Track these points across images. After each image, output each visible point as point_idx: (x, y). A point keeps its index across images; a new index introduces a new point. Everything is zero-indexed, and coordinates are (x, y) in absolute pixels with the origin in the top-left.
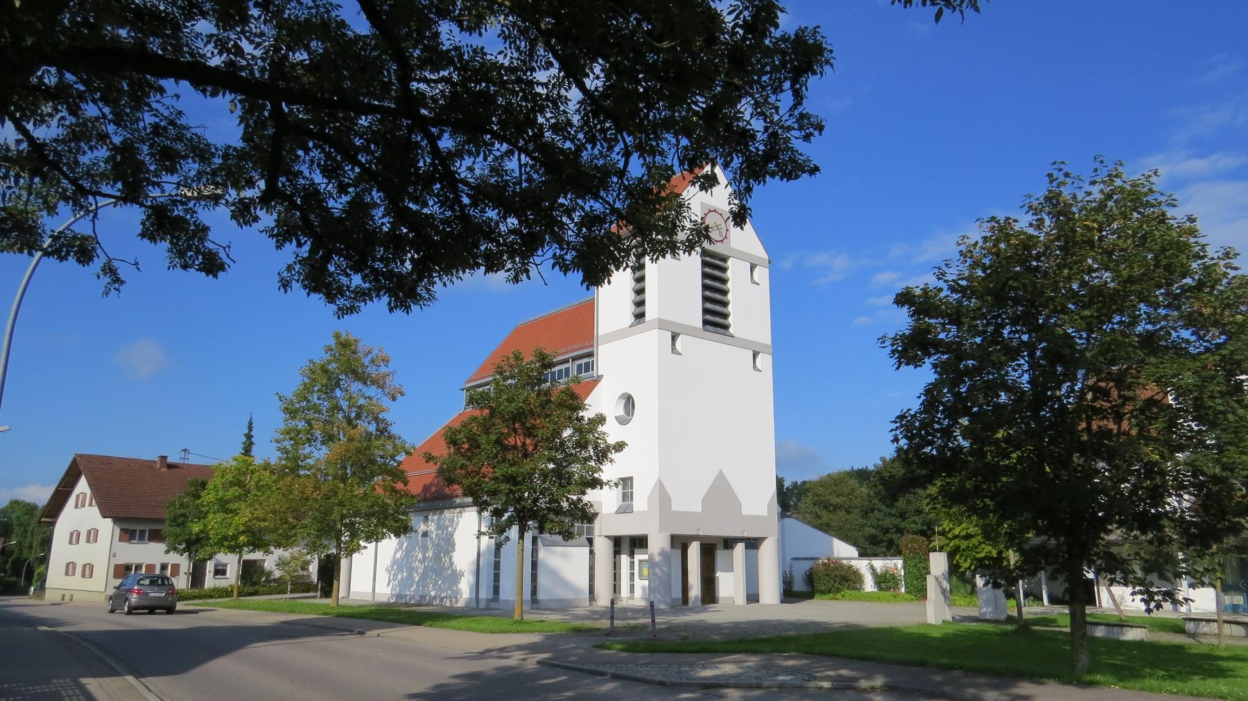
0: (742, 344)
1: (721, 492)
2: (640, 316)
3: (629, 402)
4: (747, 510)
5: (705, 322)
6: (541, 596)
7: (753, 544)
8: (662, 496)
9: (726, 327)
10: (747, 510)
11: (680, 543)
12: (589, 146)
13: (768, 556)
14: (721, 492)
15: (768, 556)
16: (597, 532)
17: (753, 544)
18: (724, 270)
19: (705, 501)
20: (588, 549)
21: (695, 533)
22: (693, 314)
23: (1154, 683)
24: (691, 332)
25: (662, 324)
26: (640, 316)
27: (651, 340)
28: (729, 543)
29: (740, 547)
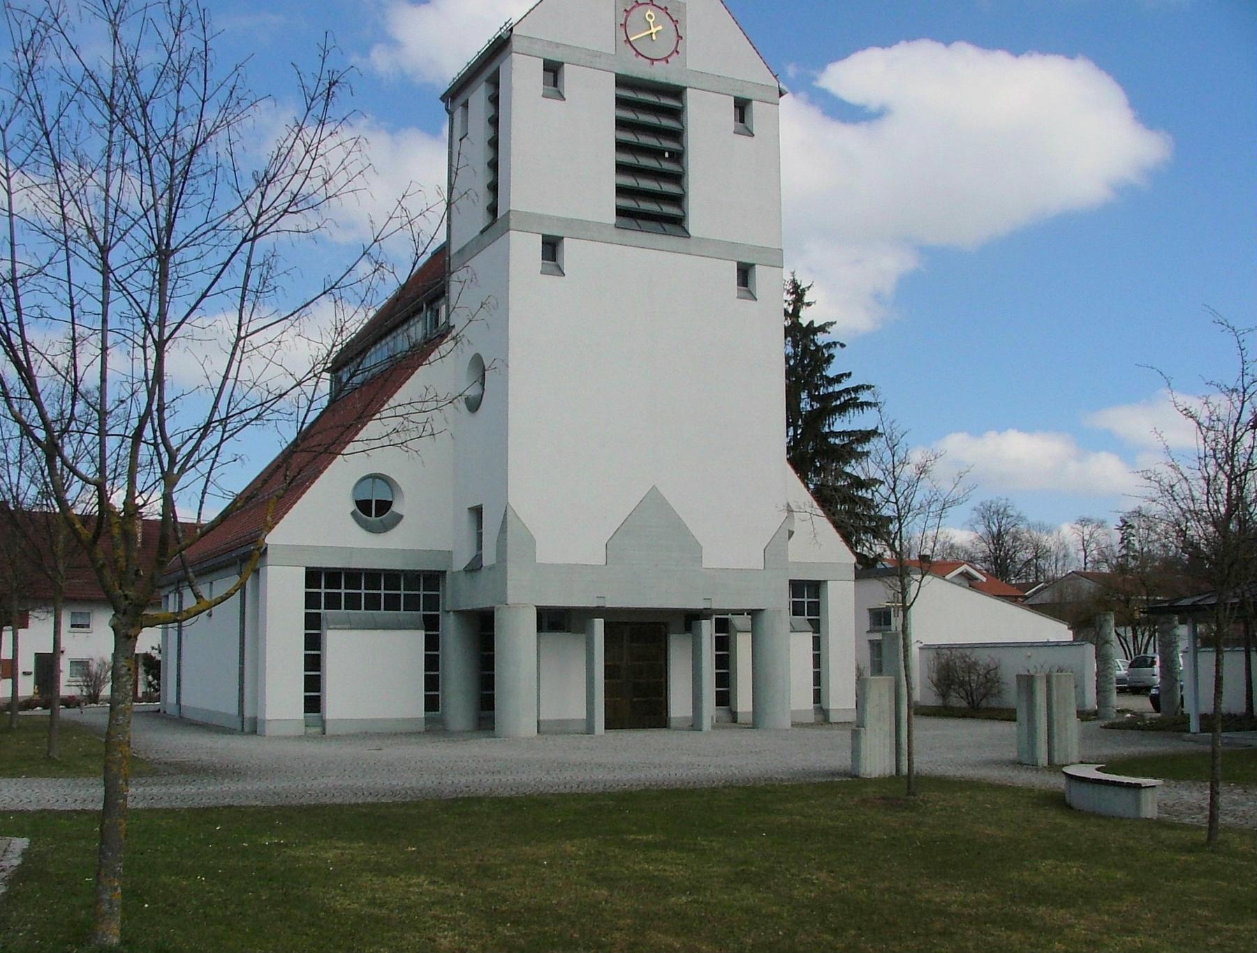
1: (654, 523)
4: (714, 558)
10: (714, 558)
14: (654, 523)
24: (586, 230)
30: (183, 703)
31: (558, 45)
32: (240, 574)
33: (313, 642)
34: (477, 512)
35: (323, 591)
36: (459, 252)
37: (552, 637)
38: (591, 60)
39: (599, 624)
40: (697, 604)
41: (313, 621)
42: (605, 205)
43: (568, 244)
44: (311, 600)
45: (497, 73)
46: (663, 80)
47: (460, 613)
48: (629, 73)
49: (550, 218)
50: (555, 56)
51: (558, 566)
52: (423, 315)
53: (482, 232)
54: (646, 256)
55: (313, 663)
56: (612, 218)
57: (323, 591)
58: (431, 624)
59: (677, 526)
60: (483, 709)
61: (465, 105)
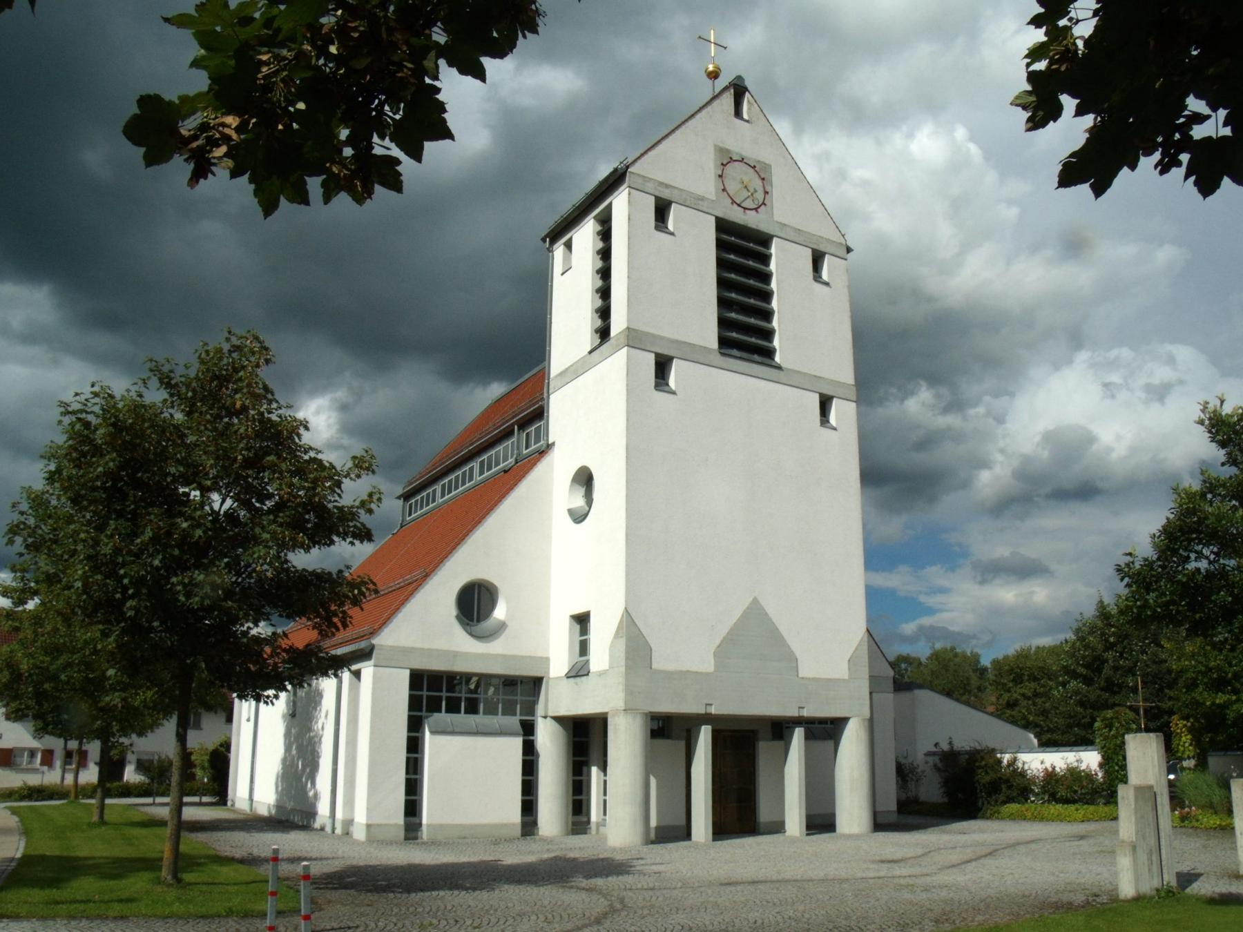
0: (799, 381)
1: (755, 635)
2: (604, 333)
3: (585, 479)
4: (808, 669)
5: (724, 343)
6: (106, 817)
7: (826, 731)
8: (635, 644)
9: (769, 353)
10: (808, 669)
11: (667, 730)
12: (1231, 715)
13: (851, 755)
14: (755, 635)
15: (851, 755)
16: (540, 709)
17: (826, 731)
18: (765, 259)
19: (722, 653)
20: (517, 743)
21: (700, 710)
22: (700, 321)
23: (1046, 641)
24: (694, 354)
25: (634, 339)
26: (604, 333)
27: (616, 365)
28: (780, 729)
29: (798, 735)
30: (255, 798)
31: (667, 186)
32: (336, 676)
33: (414, 746)
34: (582, 620)
35: (425, 693)
36: (561, 374)
37: (662, 743)
38: (695, 203)
39: (705, 737)
40: (792, 712)
41: (415, 725)
42: (709, 336)
43: (676, 364)
44: (414, 703)
45: (571, 239)
46: (754, 226)
47: (560, 720)
48: (726, 217)
49: (662, 338)
50: (665, 194)
51: (671, 673)
52: (514, 439)
53: (590, 352)
54: (738, 383)
55: (414, 766)
56: (714, 344)
57: (425, 693)
58: (528, 729)
59: (774, 637)
60: (416, 780)
61: (569, 245)
